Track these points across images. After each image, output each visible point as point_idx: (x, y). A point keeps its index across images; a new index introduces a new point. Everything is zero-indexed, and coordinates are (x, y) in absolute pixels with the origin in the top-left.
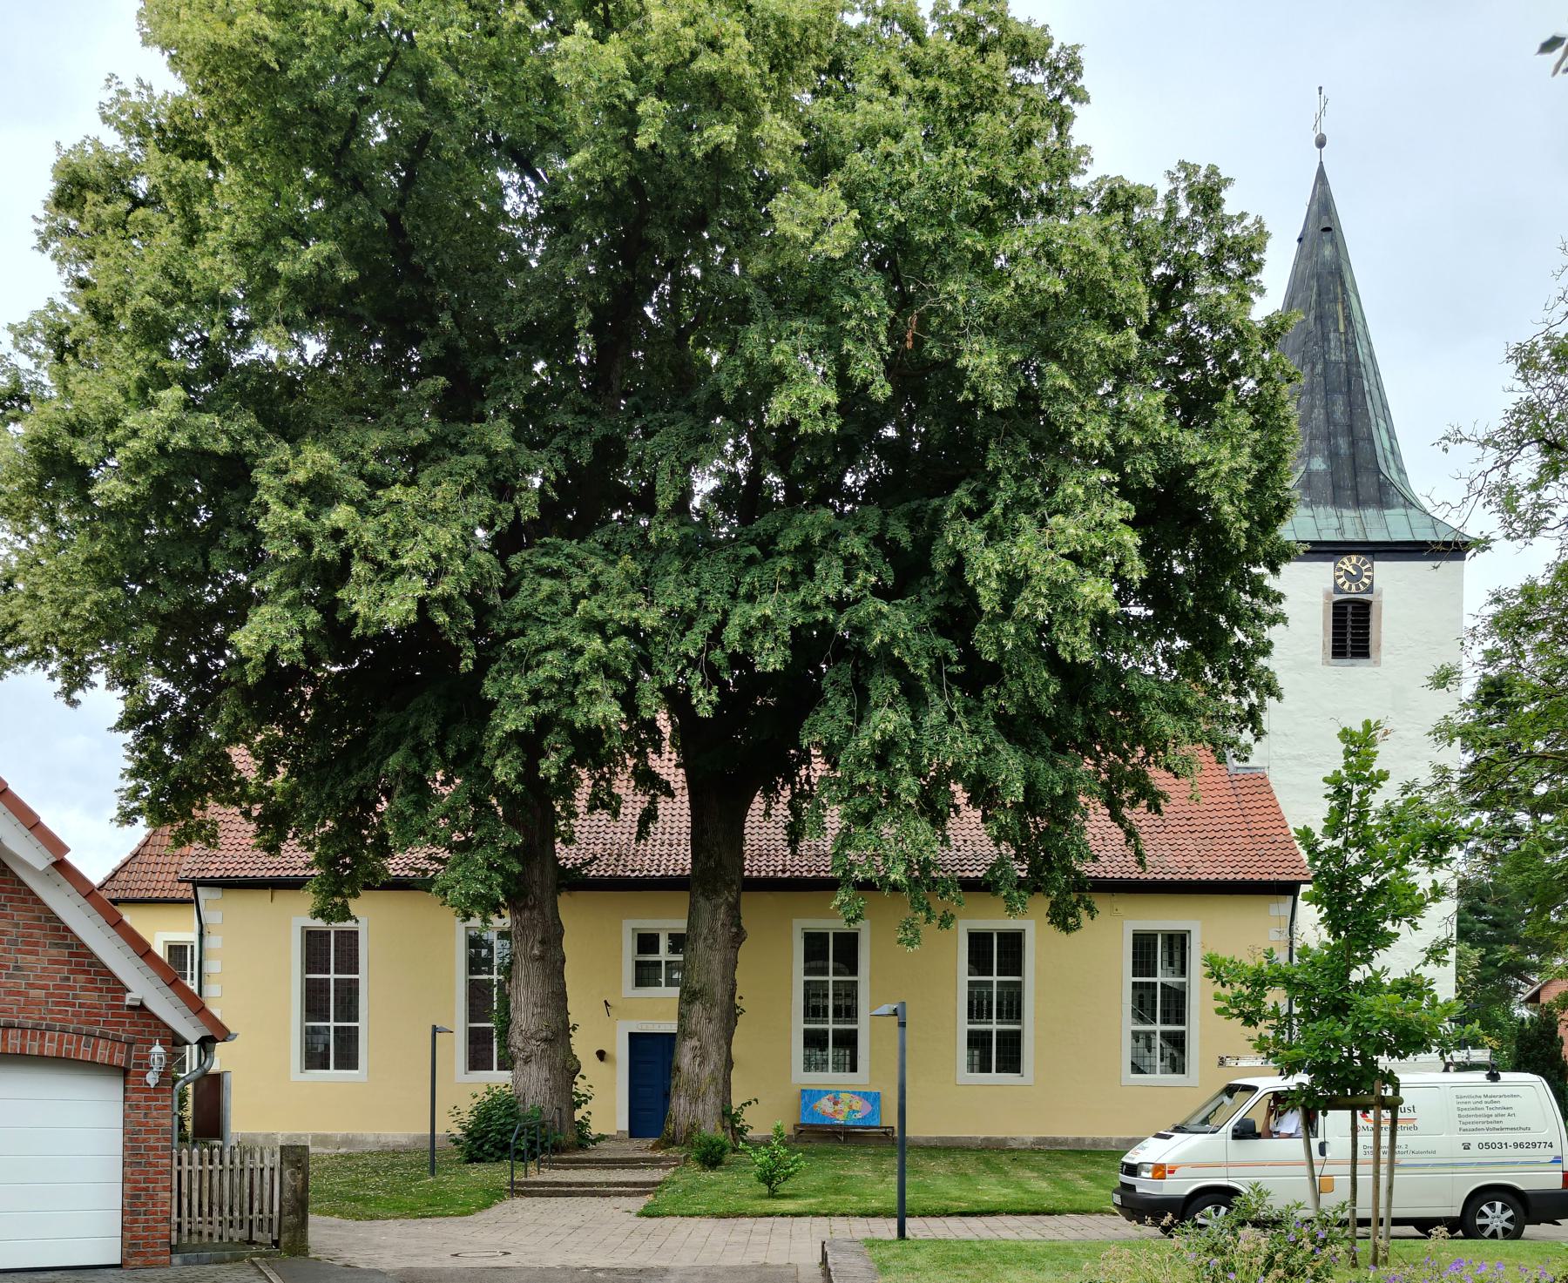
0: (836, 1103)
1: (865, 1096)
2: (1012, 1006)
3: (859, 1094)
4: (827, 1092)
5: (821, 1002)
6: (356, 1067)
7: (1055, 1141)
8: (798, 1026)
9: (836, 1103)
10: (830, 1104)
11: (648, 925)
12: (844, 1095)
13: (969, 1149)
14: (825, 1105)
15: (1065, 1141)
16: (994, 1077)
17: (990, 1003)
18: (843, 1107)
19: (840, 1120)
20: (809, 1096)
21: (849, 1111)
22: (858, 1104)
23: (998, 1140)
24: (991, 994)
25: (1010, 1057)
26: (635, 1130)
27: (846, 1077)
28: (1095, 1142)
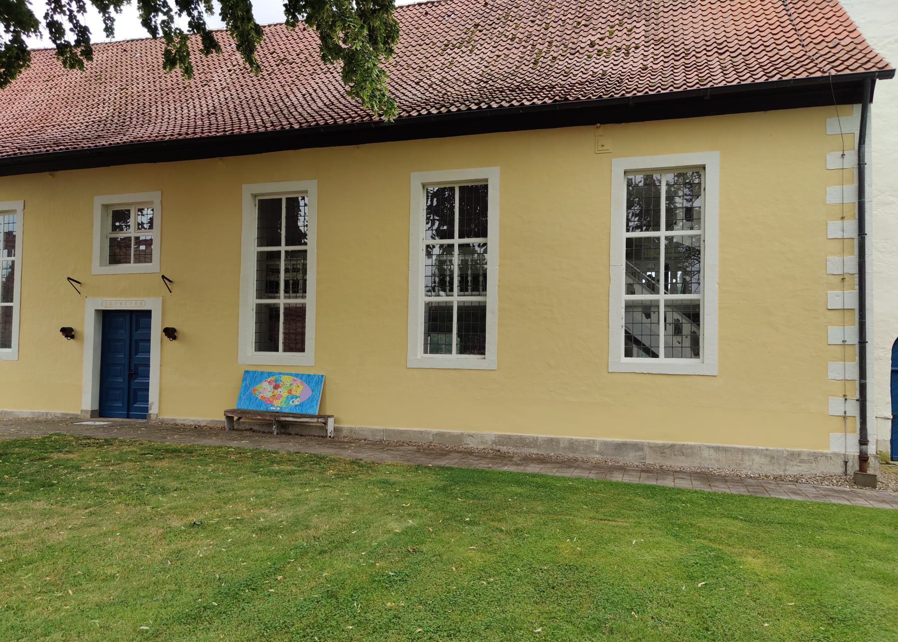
0: (276, 387)
1: (308, 379)
2: (475, 280)
3: (297, 375)
4: (270, 374)
5: (291, 275)
6: (302, 350)
7: (521, 442)
8: (249, 300)
9: (276, 387)
10: (269, 388)
11: (119, 199)
12: (285, 379)
13: (535, 459)
14: (265, 389)
15: (534, 443)
16: (454, 359)
17: (452, 279)
18: (283, 392)
19: (278, 405)
20: (252, 377)
21: (286, 398)
22: (300, 389)
23: (452, 436)
24: (452, 272)
25: (473, 339)
26: (103, 410)
27: (293, 358)
28: (572, 445)
